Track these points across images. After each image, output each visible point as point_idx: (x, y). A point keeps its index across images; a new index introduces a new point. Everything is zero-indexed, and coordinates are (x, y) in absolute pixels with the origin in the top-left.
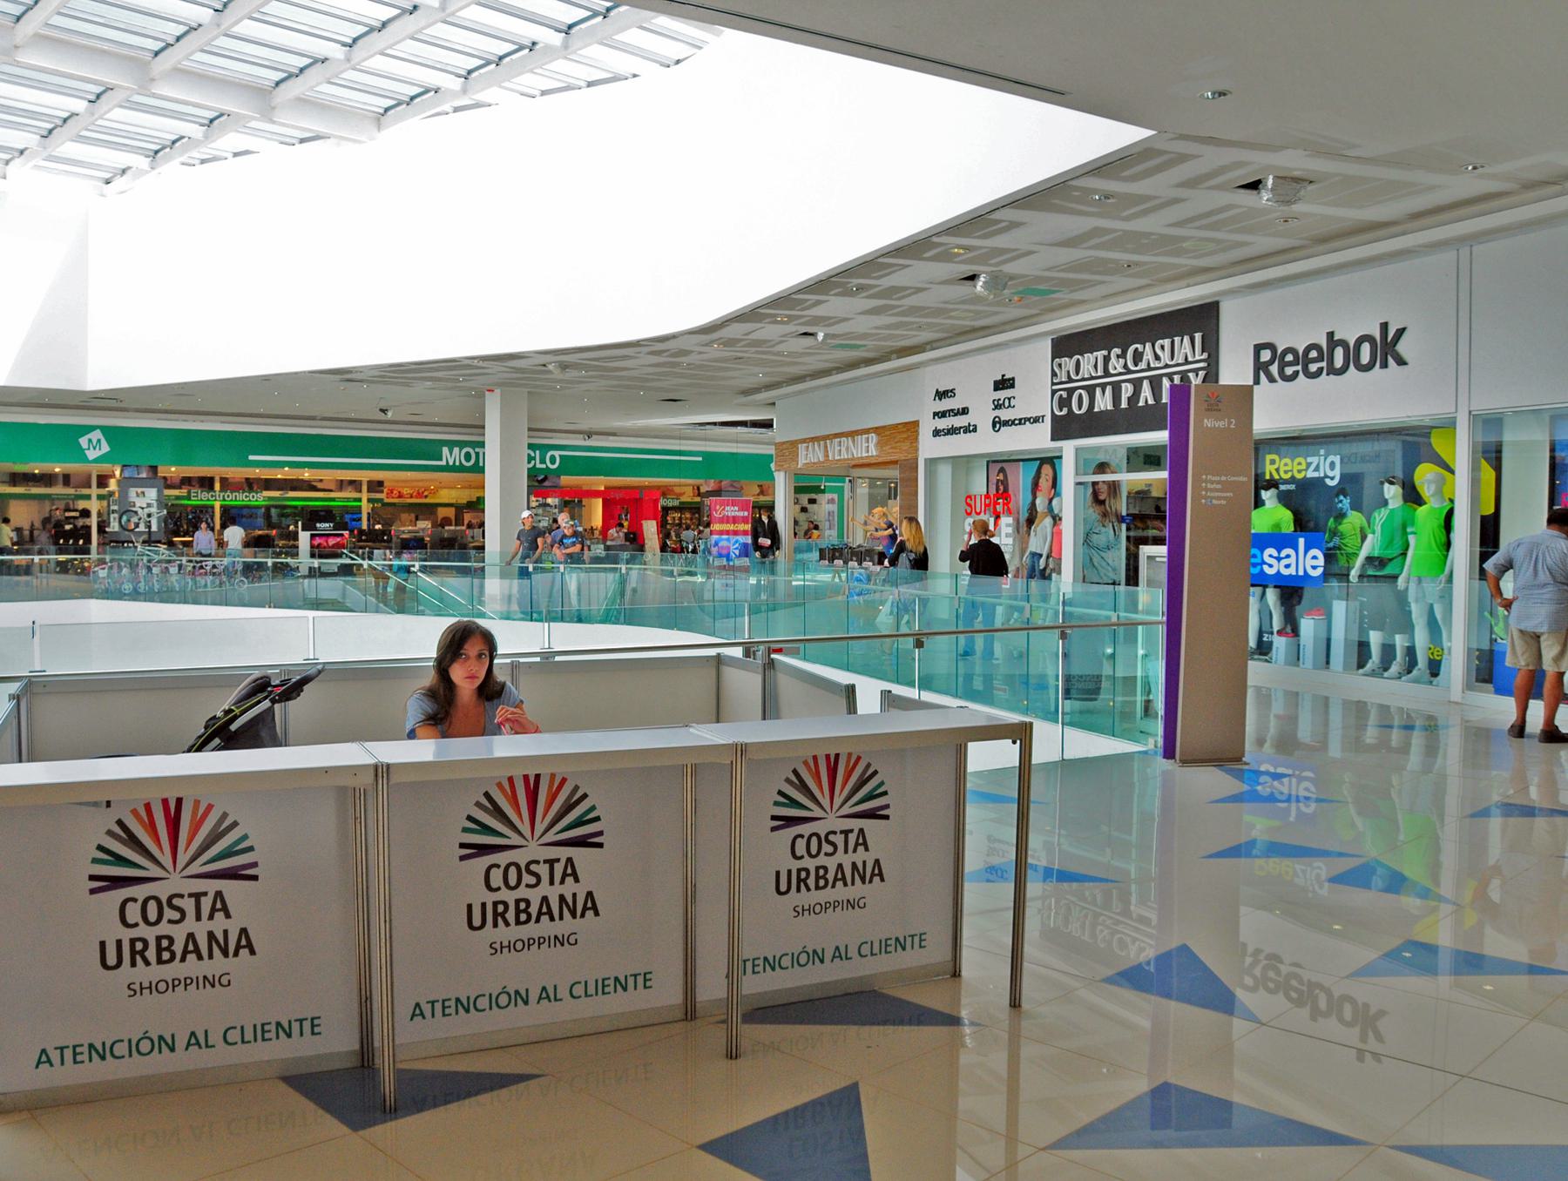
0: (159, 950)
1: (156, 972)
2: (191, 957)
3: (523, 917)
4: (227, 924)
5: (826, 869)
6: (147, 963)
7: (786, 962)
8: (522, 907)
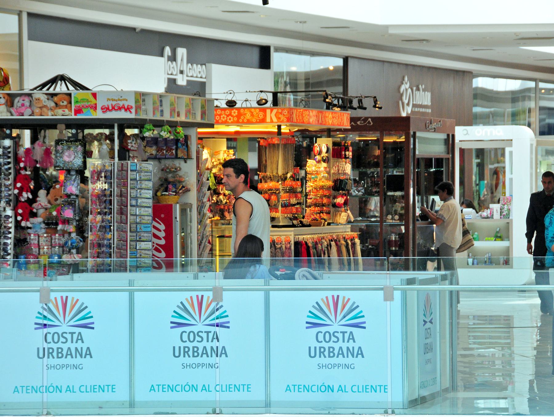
0: (194, 352)
1: (56, 361)
2: (69, 357)
3: (332, 354)
4: (218, 344)
5: (62, 349)
6: (53, 358)
7: (178, 388)
8: (60, 351)
